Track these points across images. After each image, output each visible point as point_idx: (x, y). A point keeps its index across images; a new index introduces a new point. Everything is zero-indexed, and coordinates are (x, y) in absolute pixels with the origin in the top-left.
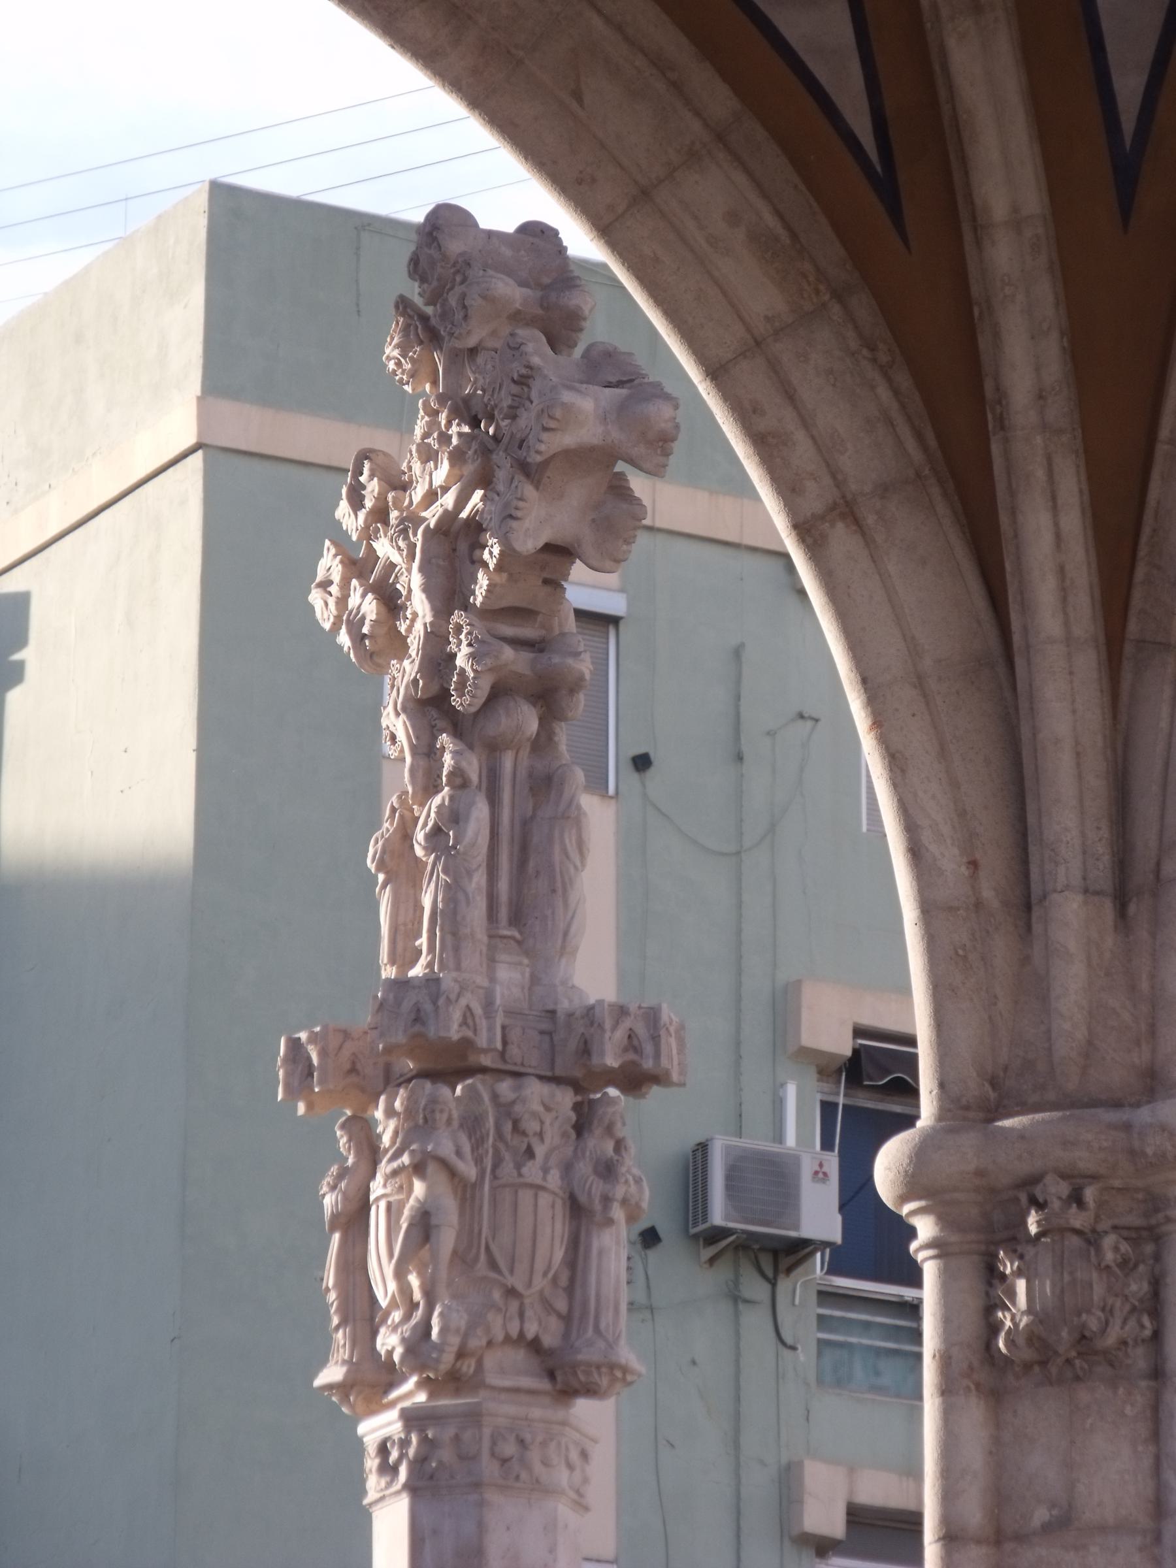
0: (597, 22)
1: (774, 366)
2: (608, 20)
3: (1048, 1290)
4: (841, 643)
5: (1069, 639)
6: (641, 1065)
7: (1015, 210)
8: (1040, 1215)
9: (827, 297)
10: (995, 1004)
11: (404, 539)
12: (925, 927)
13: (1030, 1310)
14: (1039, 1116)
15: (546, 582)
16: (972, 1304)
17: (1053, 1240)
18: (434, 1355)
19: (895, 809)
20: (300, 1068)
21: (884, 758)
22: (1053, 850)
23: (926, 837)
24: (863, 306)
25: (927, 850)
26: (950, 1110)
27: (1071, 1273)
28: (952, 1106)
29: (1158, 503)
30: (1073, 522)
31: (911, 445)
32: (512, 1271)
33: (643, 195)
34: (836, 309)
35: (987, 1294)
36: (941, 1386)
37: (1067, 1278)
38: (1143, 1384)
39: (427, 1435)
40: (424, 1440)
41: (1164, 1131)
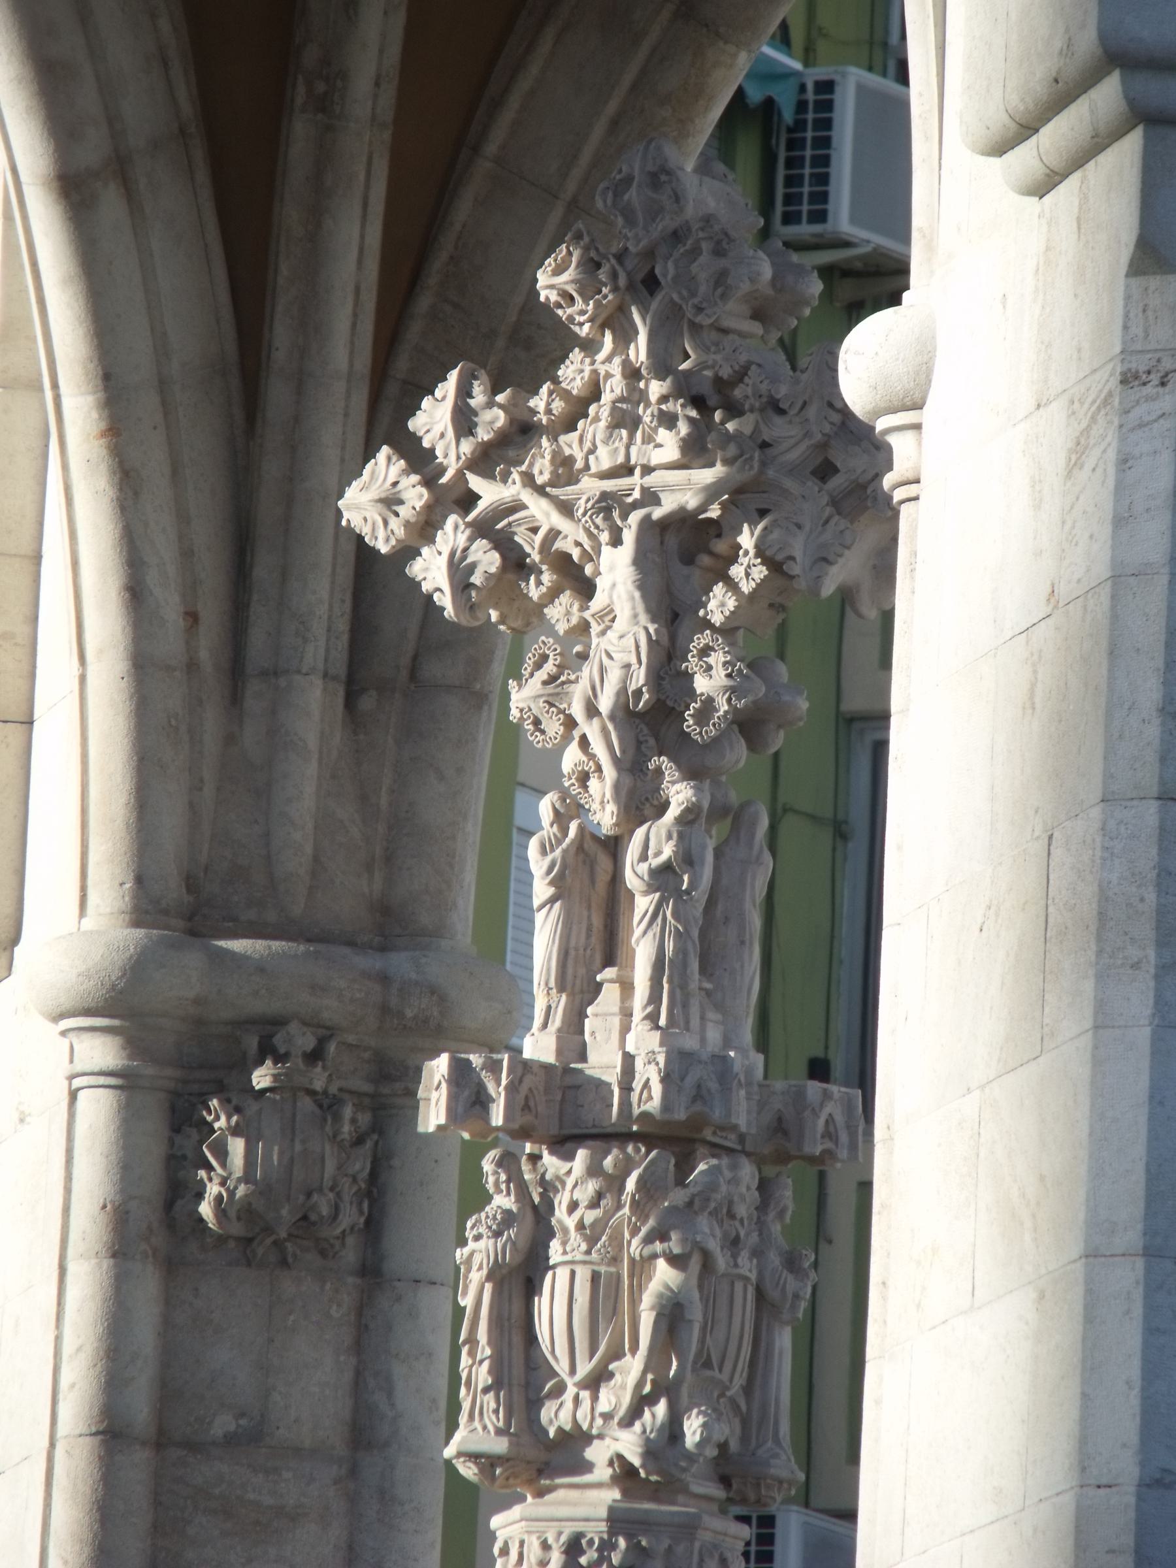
3: (275, 1157)
4: (84, 325)
6: (836, 1154)
8: (279, 1068)
10: (201, 789)
11: (605, 519)
12: (137, 685)
13: (247, 1178)
14: (276, 945)
16: (156, 1151)
17: (282, 1098)
18: (683, 1464)
19: (116, 536)
20: (466, 1093)
21: (114, 473)
22: (303, 623)
23: (152, 578)
25: (151, 594)
26: (147, 912)
27: (303, 1142)
28: (150, 907)
29: (464, 226)
32: (720, 1371)
35: (171, 1143)
36: (114, 1245)
37: (298, 1147)
38: (351, 1280)
39: (639, 1542)
40: (635, 1548)
41: (433, 993)
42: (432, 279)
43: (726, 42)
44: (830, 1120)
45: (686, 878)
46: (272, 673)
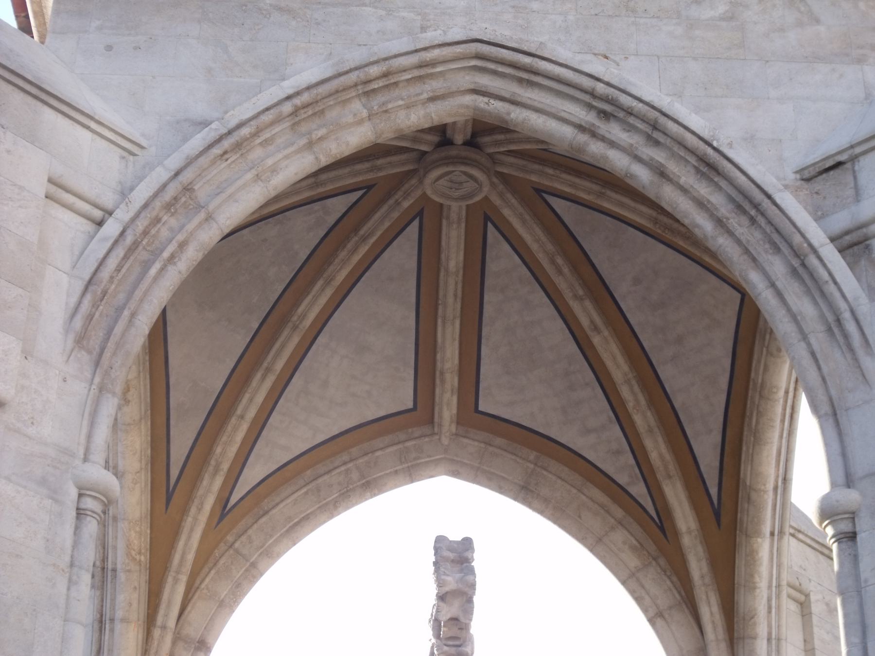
0: (584, 498)
1: (638, 580)
2: (587, 497)
5: (717, 640)
7: (689, 528)
9: (651, 560)
15: (459, 629)
24: (662, 561)
30: (715, 609)
31: (677, 596)
33: (600, 540)
34: (654, 563)
43: (753, 538)
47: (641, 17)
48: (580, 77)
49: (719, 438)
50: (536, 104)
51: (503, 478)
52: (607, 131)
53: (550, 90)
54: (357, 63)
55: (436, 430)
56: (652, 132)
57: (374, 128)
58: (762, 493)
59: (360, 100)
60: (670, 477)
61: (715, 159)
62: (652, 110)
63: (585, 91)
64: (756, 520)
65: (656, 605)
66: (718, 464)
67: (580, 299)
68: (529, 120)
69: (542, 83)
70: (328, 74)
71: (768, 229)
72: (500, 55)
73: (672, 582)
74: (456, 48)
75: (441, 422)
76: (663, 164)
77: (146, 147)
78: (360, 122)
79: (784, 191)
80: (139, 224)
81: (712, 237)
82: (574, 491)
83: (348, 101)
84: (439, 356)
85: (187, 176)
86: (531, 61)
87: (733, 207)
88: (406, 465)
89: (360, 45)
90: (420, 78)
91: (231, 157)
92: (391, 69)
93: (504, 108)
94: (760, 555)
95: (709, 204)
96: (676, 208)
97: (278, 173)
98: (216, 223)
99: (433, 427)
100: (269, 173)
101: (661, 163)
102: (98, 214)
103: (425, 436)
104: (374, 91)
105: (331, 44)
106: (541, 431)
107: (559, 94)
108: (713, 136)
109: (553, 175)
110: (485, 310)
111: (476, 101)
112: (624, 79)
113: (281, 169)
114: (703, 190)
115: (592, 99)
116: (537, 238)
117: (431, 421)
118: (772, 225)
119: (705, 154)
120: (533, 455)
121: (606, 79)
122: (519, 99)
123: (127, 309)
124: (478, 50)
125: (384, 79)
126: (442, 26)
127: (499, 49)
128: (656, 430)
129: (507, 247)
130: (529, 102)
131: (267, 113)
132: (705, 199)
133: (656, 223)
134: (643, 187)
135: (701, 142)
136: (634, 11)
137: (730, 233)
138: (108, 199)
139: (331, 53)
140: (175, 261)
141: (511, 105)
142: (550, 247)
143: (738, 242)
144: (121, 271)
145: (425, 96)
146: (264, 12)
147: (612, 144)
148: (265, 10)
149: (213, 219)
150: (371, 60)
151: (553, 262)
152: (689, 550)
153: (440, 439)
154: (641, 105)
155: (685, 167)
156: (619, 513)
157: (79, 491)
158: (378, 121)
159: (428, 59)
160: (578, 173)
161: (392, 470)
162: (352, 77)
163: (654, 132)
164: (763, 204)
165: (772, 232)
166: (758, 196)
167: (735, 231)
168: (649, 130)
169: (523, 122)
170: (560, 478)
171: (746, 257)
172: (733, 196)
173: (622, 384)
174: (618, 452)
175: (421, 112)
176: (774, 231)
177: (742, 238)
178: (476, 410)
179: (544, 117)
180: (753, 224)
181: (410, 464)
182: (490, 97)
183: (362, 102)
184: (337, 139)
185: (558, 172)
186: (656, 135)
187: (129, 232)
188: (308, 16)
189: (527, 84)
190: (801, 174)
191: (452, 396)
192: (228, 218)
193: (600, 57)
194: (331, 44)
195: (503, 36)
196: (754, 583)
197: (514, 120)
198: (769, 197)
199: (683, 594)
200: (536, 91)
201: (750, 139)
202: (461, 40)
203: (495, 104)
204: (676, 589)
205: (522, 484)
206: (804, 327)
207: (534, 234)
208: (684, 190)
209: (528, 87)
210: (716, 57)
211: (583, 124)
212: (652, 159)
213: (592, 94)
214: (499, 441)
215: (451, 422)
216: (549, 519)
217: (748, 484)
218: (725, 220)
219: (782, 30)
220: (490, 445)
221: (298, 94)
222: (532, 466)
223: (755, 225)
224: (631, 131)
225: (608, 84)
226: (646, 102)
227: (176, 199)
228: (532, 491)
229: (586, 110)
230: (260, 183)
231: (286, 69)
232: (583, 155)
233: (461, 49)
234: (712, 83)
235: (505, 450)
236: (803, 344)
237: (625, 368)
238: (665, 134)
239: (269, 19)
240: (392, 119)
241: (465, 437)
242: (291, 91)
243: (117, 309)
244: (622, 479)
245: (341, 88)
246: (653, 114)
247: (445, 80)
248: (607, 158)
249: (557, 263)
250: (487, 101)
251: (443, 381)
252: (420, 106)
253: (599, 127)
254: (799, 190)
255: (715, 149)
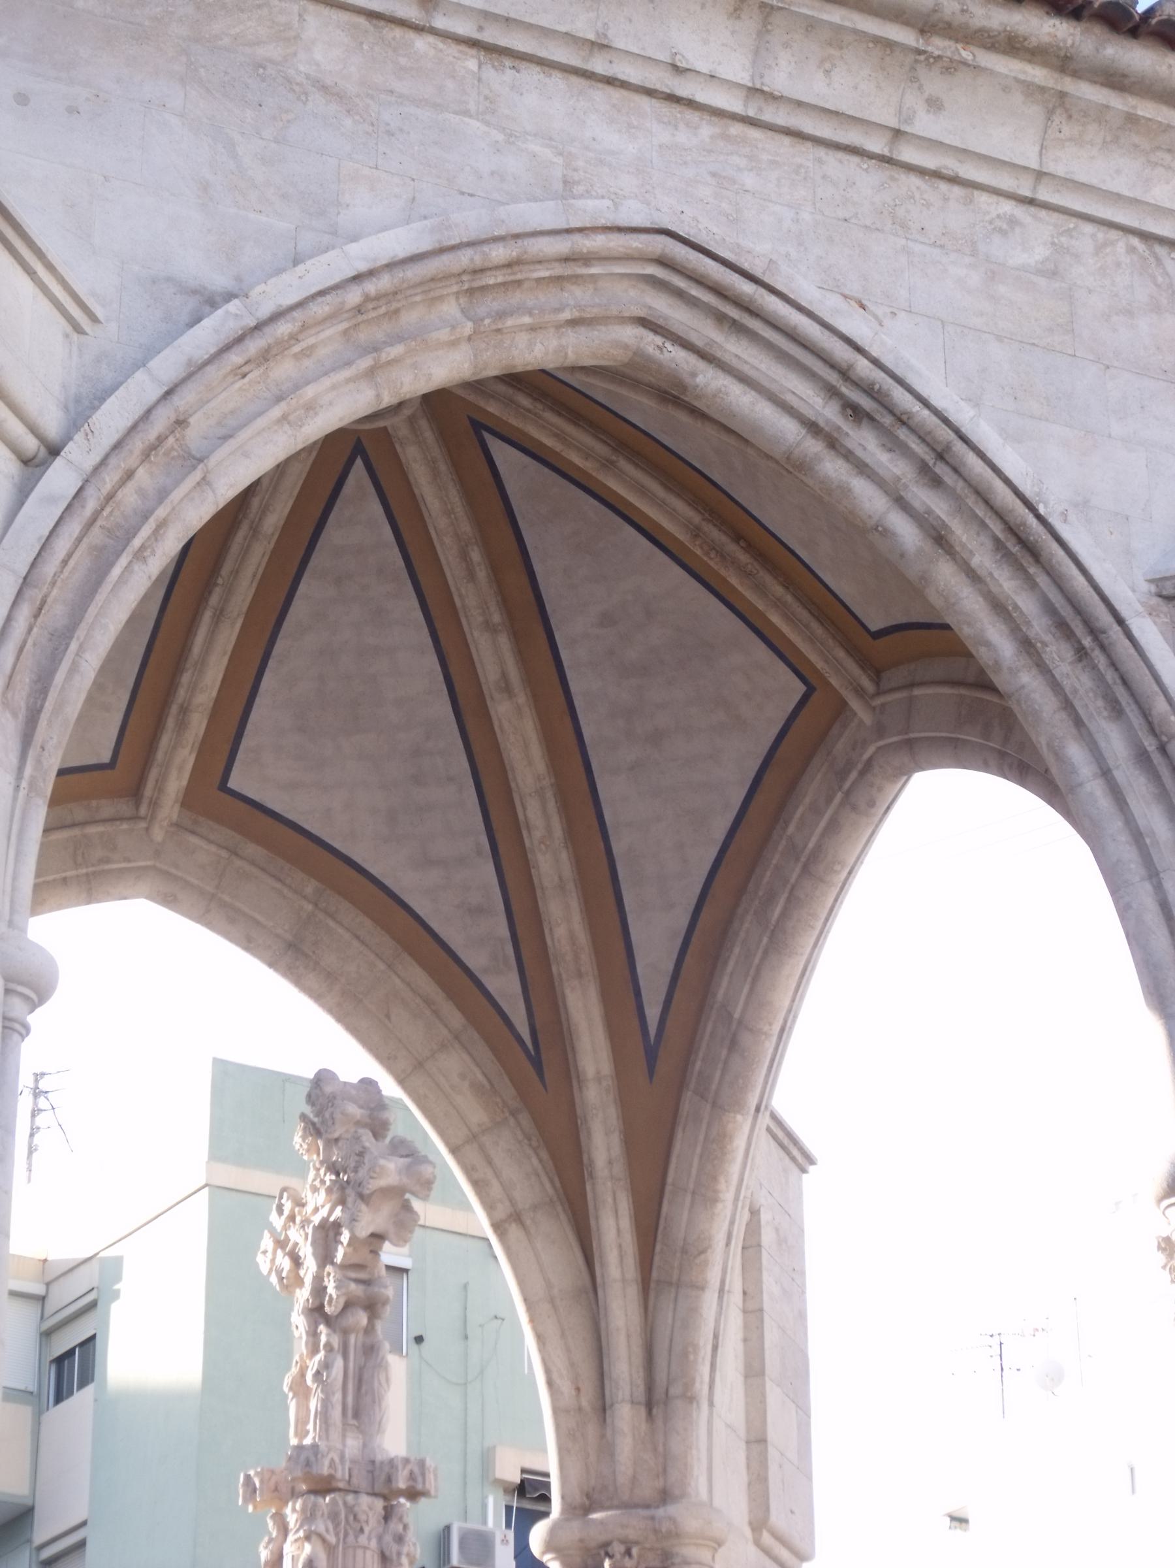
0: (397, 981)
1: (482, 1148)
2: (403, 980)
5: (624, 1280)
7: (598, 1072)
14: (610, 1513)
15: (371, 1251)
23: (555, 1376)
24: (525, 1119)
30: (626, 1223)
31: (548, 1186)
33: (419, 1065)
34: (512, 1121)
42: (659, 1237)
43: (729, 1112)
44: (332, 1460)
45: (325, 1374)
46: (612, 1405)
47: (916, 241)
48: (832, 339)
49: (684, 921)
50: (746, 369)
51: (258, 923)
52: (860, 444)
53: (769, 346)
54: (472, 235)
55: (143, 810)
56: (935, 464)
57: (475, 356)
58: (763, 1037)
59: (457, 298)
60: (580, 975)
61: (1040, 537)
62: (944, 426)
63: (832, 365)
64: (741, 1081)
65: (511, 1200)
66: (670, 966)
67: (488, 626)
68: (727, 394)
69: (761, 332)
70: (425, 245)
71: (1110, 676)
72: (703, 268)
73: (541, 1161)
74: (632, 239)
75: (158, 798)
76: (947, 525)
77: (103, 321)
78: (453, 344)
79: (1144, 617)
80: (107, 479)
81: (1010, 669)
82: (381, 966)
83: (441, 298)
84: (186, 679)
85: (185, 399)
86: (753, 291)
87: (1050, 622)
88: (84, 871)
89: (463, 193)
90: (558, 280)
91: (252, 371)
92: (525, 256)
93: (687, 363)
94: (735, 1144)
95: (1015, 612)
96: (954, 604)
97: (316, 414)
98: (213, 491)
99: (137, 805)
100: (303, 411)
101: (944, 521)
102: (31, 444)
103: (122, 819)
104: (484, 289)
105: (413, 180)
106: (337, 845)
107: (782, 357)
108: (1038, 494)
109: (529, 411)
110: (292, 610)
111: (642, 338)
112: (902, 358)
113: (322, 407)
114: (1006, 583)
115: (841, 382)
116: (449, 507)
117: (135, 793)
118: (1117, 669)
119: (1024, 524)
120: (311, 887)
121: (875, 352)
122: (719, 354)
123: (74, 640)
124: (667, 251)
125: (505, 271)
126: (598, 185)
127: (701, 256)
128: (571, 886)
129: (377, 508)
130: (735, 363)
131: (320, 299)
132: (1010, 602)
133: (696, 536)
134: (902, 556)
135: (1018, 501)
136: (904, 226)
137: (1044, 669)
138: (52, 423)
139: (414, 199)
140: (145, 554)
141: (701, 360)
142: (466, 528)
143: (1055, 686)
144: (69, 563)
145: (567, 315)
146: (297, 88)
147: (862, 468)
148: (297, 84)
149: (209, 484)
150: (496, 234)
151: (464, 556)
152: (594, 1111)
153: (147, 829)
154: (926, 412)
155: (978, 534)
156: (456, 1019)
157: (5, 985)
158: (483, 346)
159: (585, 251)
160: (576, 417)
161: (57, 876)
162: (463, 258)
163: (938, 463)
164: (1111, 633)
165: (1115, 683)
166: (1104, 618)
167: (1054, 668)
168: (930, 458)
169: (715, 396)
170: (357, 937)
171: (1063, 715)
172: (1057, 605)
173: (530, 795)
174: (478, 911)
175: (553, 343)
176: (1119, 681)
177: (1065, 683)
178: (223, 786)
179: (753, 393)
180: (1080, 660)
181: (91, 869)
182: (666, 338)
183: (460, 305)
184: (415, 366)
185: (539, 406)
186: (941, 469)
187: (90, 491)
188: (373, 115)
189: (730, 327)
190: (1157, 586)
191: (190, 754)
192: (231, 486)
193: (853, 303)
194: (413, 180)
195: (711, 234)
196: (716, 1191)
197: (699, 388)
198: (1120, 621)
199: (558, 1185)
200: (744, 342)
201: (1083, 505)
202: (643, 226)
203: (673, 352)
204: (547, 1173)
205: (289, 937)
206: (1156, 858)
207: (445, 499)
208: (973, 576)
209: (731, 333)
210: (1032, 341)
211: (822, 423)
212: (929, 511)
213: (845, 373)
214: (252, 849)
215: (176, 802)
216: (330, 1011)
217: (737, 1016)
218: (1039, 645)
219: (1129, 313)
220: (237, 855)
221: (371, 273)
222: (310, 907)
223: (1084, 662)
224: (894, 451)
225: (876, 362)
226: (936, 409)
227: (161, 439)
228: (306, 956)
229: (823, 396)
230: (286, 427)
231: (339, 213)
232: (805, 474)
233: (641, 243)
234: (1025, 391)
235: (263, 870)
236: (1148, 886)
237: (541, 766)
238: (956, 470)
239: (305, 103)
240: (505, 345)
241: (193, 832)
242: (363, 267)
243: (52, 635)
244: (475, 960)
245: (440, 276)
246: (945, 434)
247: (595, 289)
248: (850, 490)
249: (471, 560)
250: (660, 344)
251: (182, 725)
252: (552, 330)
253: (847, 434)
254: (1154, 613)
255: (1038, 517)
